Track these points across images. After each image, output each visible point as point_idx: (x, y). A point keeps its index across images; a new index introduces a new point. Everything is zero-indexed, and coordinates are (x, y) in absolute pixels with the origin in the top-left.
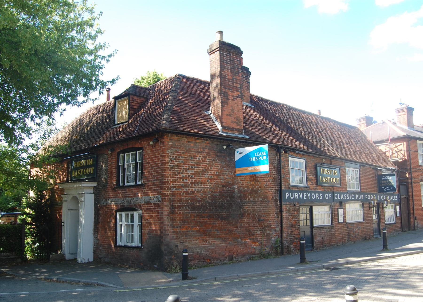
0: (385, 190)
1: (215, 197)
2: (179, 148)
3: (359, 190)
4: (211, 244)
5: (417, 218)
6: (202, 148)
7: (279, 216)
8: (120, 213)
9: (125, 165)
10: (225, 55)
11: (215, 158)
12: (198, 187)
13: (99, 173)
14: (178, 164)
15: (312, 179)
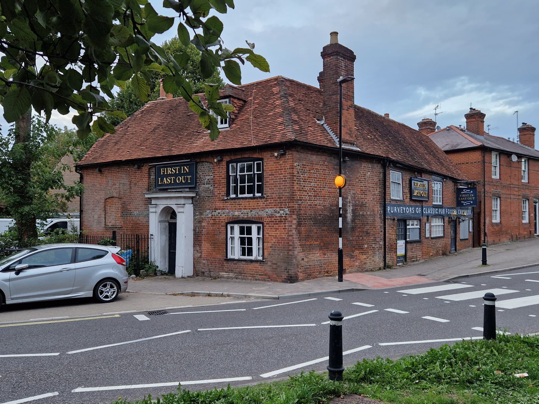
0: (464, 204)
1: (333, 210)
2: (305, 160)
3: (441, 204)
4: (329, 257)
5: (488, 234)
6: (323, 161)
7: (383, 230)
8: (232, 225)
9: (238, 175)
10: (342, 60)
11: (333, 171)
12: (320, 201)
13: (198, 183)
14: (303, 177)
15: (407, 193)
